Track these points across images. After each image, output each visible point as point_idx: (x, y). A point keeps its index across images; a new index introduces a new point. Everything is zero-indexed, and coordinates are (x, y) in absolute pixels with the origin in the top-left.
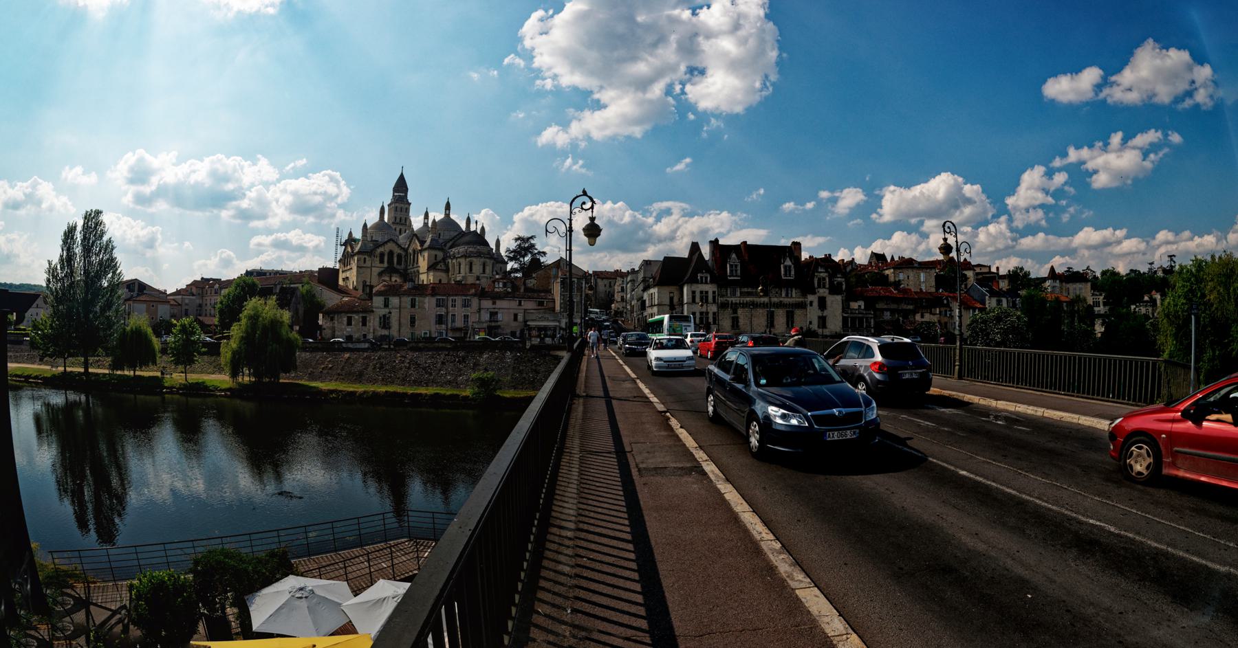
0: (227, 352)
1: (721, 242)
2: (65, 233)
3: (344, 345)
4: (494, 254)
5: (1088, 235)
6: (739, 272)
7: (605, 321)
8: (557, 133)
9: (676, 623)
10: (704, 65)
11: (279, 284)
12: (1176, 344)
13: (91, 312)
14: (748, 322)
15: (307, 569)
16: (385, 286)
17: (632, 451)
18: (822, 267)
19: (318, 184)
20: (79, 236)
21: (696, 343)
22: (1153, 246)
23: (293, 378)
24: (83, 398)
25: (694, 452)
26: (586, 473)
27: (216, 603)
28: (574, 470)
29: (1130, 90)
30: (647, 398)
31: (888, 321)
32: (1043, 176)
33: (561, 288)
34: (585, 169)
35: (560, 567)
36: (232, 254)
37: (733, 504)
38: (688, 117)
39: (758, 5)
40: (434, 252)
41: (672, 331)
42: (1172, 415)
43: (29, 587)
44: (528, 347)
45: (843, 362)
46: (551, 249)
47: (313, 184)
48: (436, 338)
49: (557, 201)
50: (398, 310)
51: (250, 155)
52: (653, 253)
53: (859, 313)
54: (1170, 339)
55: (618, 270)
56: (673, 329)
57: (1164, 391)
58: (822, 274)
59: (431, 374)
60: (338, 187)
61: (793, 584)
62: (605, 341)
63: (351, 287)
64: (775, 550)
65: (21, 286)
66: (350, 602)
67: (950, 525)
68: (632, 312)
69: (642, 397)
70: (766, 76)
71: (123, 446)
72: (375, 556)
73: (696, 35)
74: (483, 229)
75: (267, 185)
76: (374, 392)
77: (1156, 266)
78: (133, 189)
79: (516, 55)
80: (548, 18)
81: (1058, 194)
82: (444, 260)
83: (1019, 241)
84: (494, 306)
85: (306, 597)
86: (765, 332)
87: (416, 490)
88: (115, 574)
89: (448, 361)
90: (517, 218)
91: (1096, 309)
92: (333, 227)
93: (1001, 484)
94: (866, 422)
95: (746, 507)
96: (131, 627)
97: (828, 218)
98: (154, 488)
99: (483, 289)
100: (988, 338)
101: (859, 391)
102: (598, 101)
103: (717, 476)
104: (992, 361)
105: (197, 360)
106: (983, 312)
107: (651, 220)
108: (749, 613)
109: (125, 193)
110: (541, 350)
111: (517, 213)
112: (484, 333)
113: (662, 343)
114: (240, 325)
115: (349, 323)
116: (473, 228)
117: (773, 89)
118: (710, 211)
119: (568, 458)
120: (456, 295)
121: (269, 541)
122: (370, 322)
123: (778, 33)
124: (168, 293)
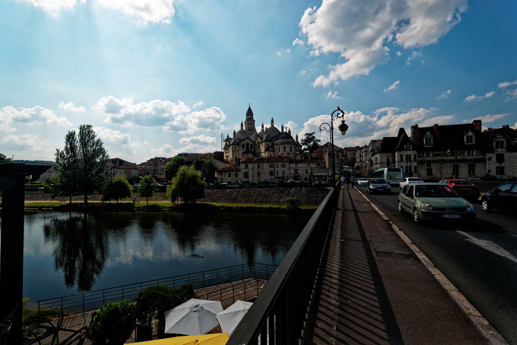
0: (170, 190)
1: (420, 126)
2: (67, 136)
3: (227, 186)
6: (432, 143)
8: (323, 79)
11: (195, 159)
13: (89, 174)
14: (439, 172)
15: (201, 295)
16: (245, 159)
17: (371, 241)
18: (499, 135)
19: (210, 113)
20: (77, 137)
23: (203, 201)
24: (83, 215)
25: (410, 246)
27: (147, 317)
28: (337, 246)
30: (378, 213)
34: (338, 96)
35: (330, 300)
36: (170, 146)
37: (442, 284)
38: (397, 55)
40: (267, 143)
43: (10, 328)
44: (313, 185)
46: (323, 138)
47: (208, 113)
48: (270, 182)
49: (324, 115)
51: (175, 100)
52: (377, 136)
56: (390, 176)
59: (267, 198)
60: (220, 114)
63: (230, 160)
65: (35, 162)
66: (221, 313)
68: (366, 167)
71: (106, 238)
72: (236, 287)
74: (289, 131)
75: (185, 114)
76: (241, 207)
78: (110, 116)
79: (299, 39)
80: (314, 12)
82: (272, 146)
84: (296, 167)
85: (198, 311)
87: (260, 253)
88: (84, 308)
90: (305, 124)
92: (220, 133)
95: (453, 287)
96: (86, 340)
98: (123, 257)
99: (291, 159)
102: (344, 57)
103: (427, 262)
105: (153, 195)
107: (375, 119)
109: (106, 117)
110: (320, 187)
111: (306, 122)
114: (177, 178)
115: (229, 176)
116: (285, 130)
117: (462, 19)
118: (411, 109)
119: (334, 240)
120: (279, 162)
121: (184, 280)
122: (239, 175)
124: (137, 164)
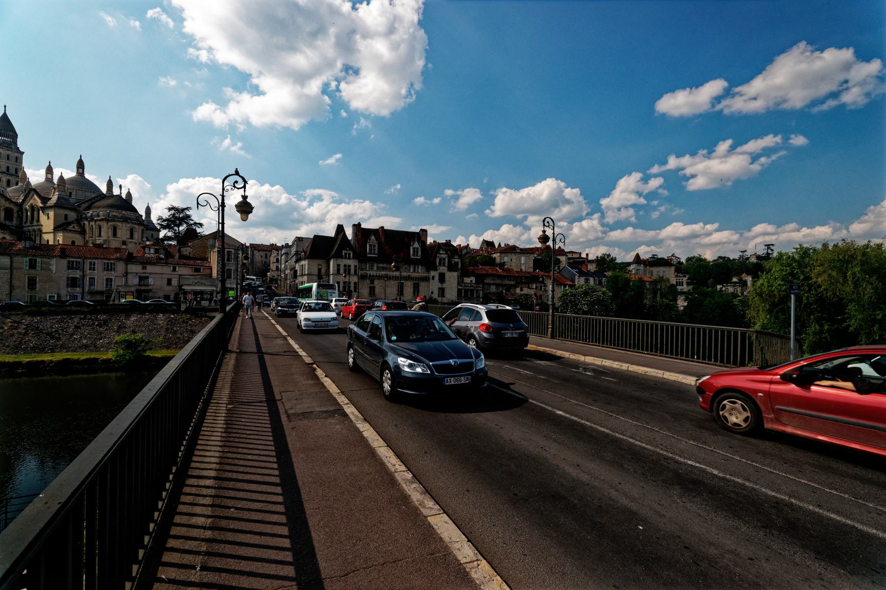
1: (363, 226)
4: (143, 221)
5: (678, 229)
7: (259, 286)
9: (322, 564)
10: (358, 65)
12: (771, 318)
18: (443, 249)
21: (340, 307)
22: (748, 237)
25: (337, 397)
26: (237, 423)
29: (755, 99)
30: (297, 352)
31: (493, 293)
32: (639, 181)
33: (218, 257)
34: (244, 151)
37: (370, 441)
39: (414, 9)
40: (63, 212)
41: (319, 296)
42: (769, 377)
45: (457, 323)
48: (67, 301)
50: (8, 271)
52: (306, 231)
53: (471, 286)
54: (762, 315)
55: (273, 244)
56: (321, 295)
57: (757, 356)
58: (442, 256)
61: (425, 512)
62: (259, 304)
64: (408, 479)
67: (553, 456)
68: (286, 279)
69: (292, 352)
70: (412, 85)
73: (354, 32)
77: (748, 254)
81: (652, 195)
82: (78, 221)
83: (608, 234)
86: (396, 299)
89: (83, 325)
90: (171, 188)
91: (679, 288)
93: (594, 424)
94: (476, 370)
97: (450, 212)
100: (576, 308)
101: (470, 346)
103: (356, 417)
104: (580, 325)
106: (573, 288)
107: (304, 204)
108: (389, 544)
112: (132, 297)
113: (311, 306)
116: (116, 191)
117: (416, 97)
120: (95, 258)
123: (427, 41)
